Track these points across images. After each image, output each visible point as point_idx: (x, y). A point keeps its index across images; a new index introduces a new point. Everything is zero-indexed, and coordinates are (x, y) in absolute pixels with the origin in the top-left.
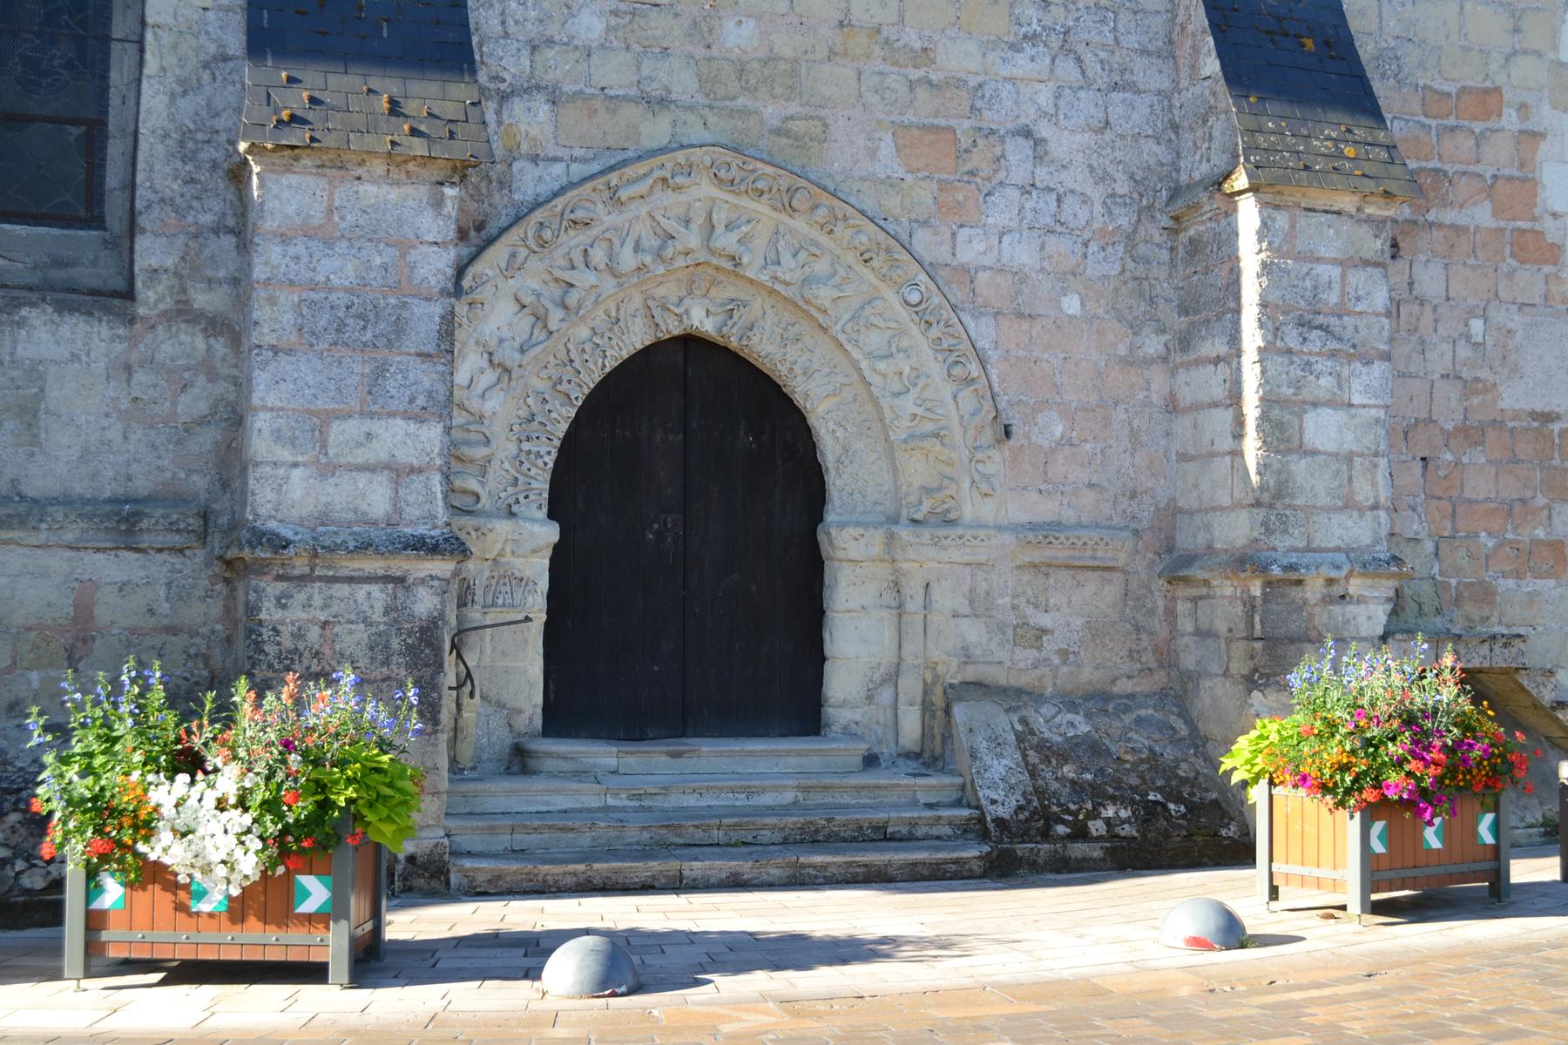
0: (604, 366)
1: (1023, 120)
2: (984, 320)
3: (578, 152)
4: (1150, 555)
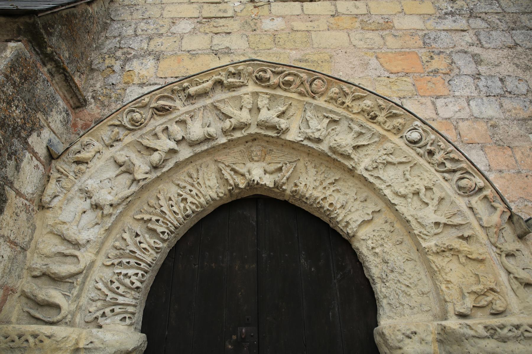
0: (185, 209)
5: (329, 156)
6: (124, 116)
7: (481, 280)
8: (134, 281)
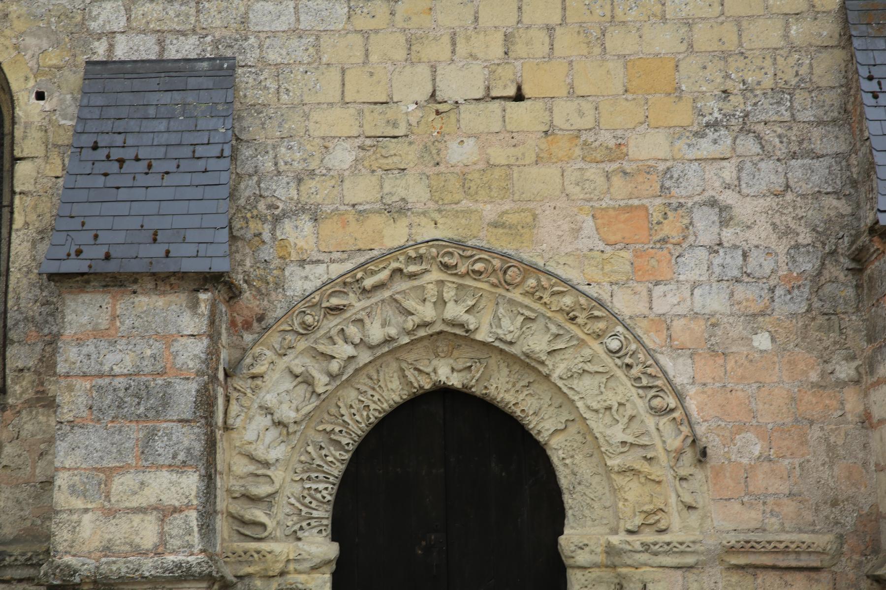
0: (368, 418)
1: (710, 193)
2: (681, 360)
3: (336, 255)
4: (856, 557)
5: (521, 360)
6: (295, 319)
7: (654, 500)
8: (326, 495)
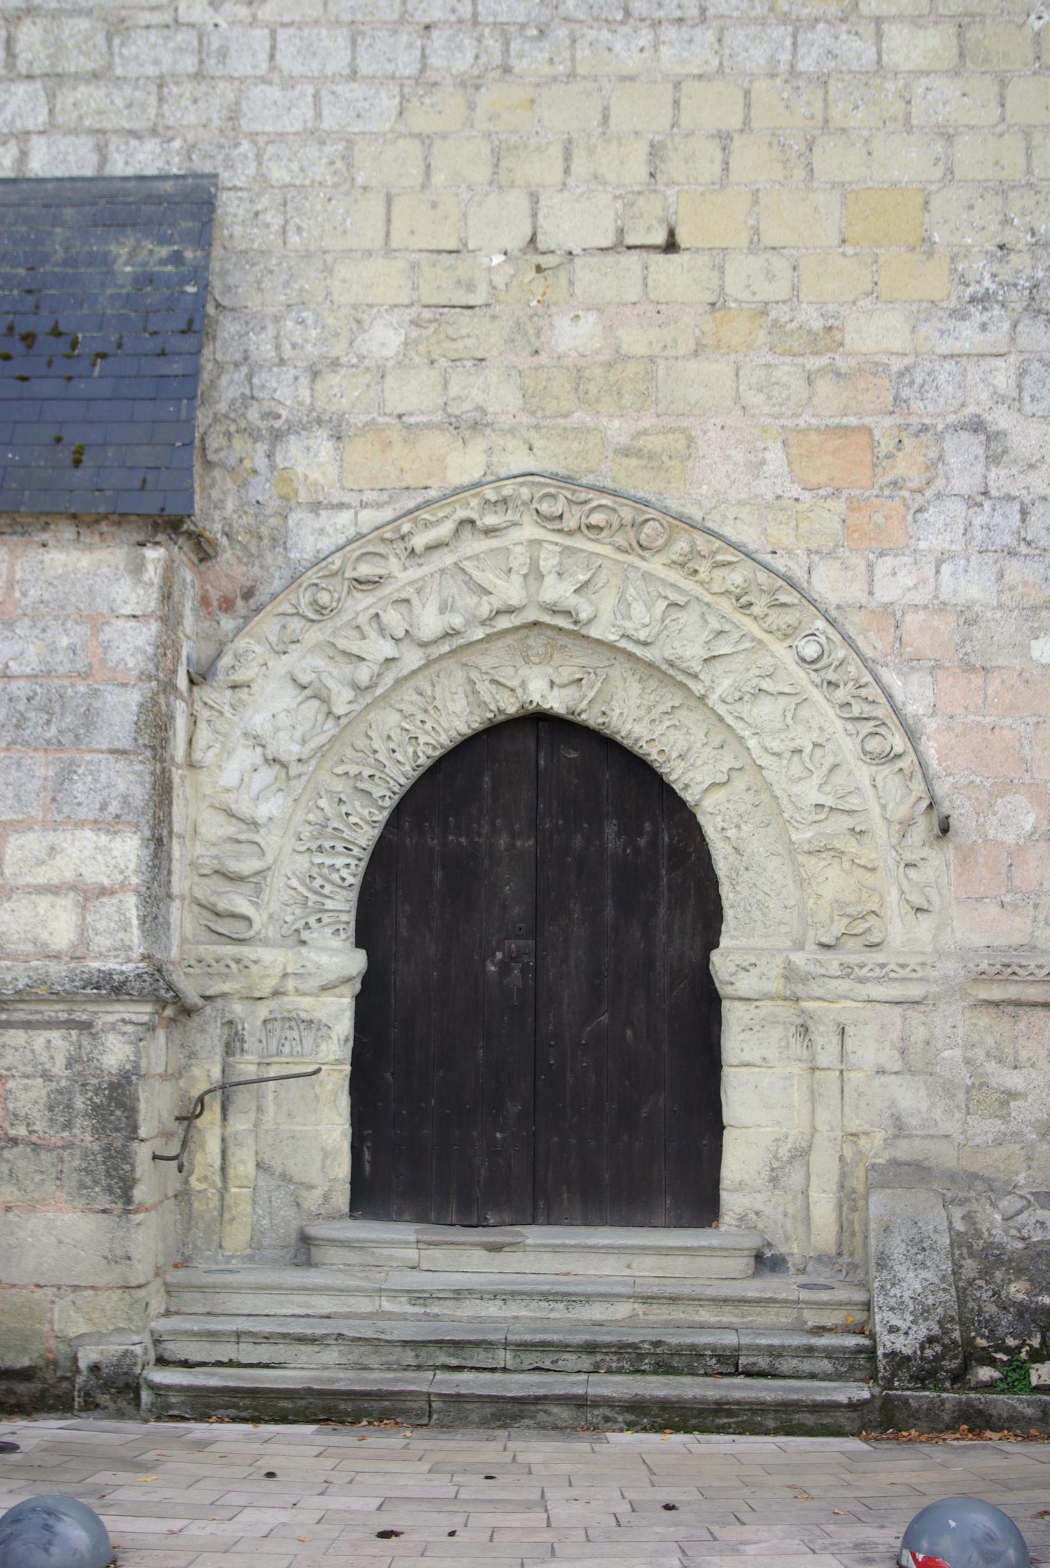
1: (971, 409)
2: (915, 677)
3: (369, 496)
